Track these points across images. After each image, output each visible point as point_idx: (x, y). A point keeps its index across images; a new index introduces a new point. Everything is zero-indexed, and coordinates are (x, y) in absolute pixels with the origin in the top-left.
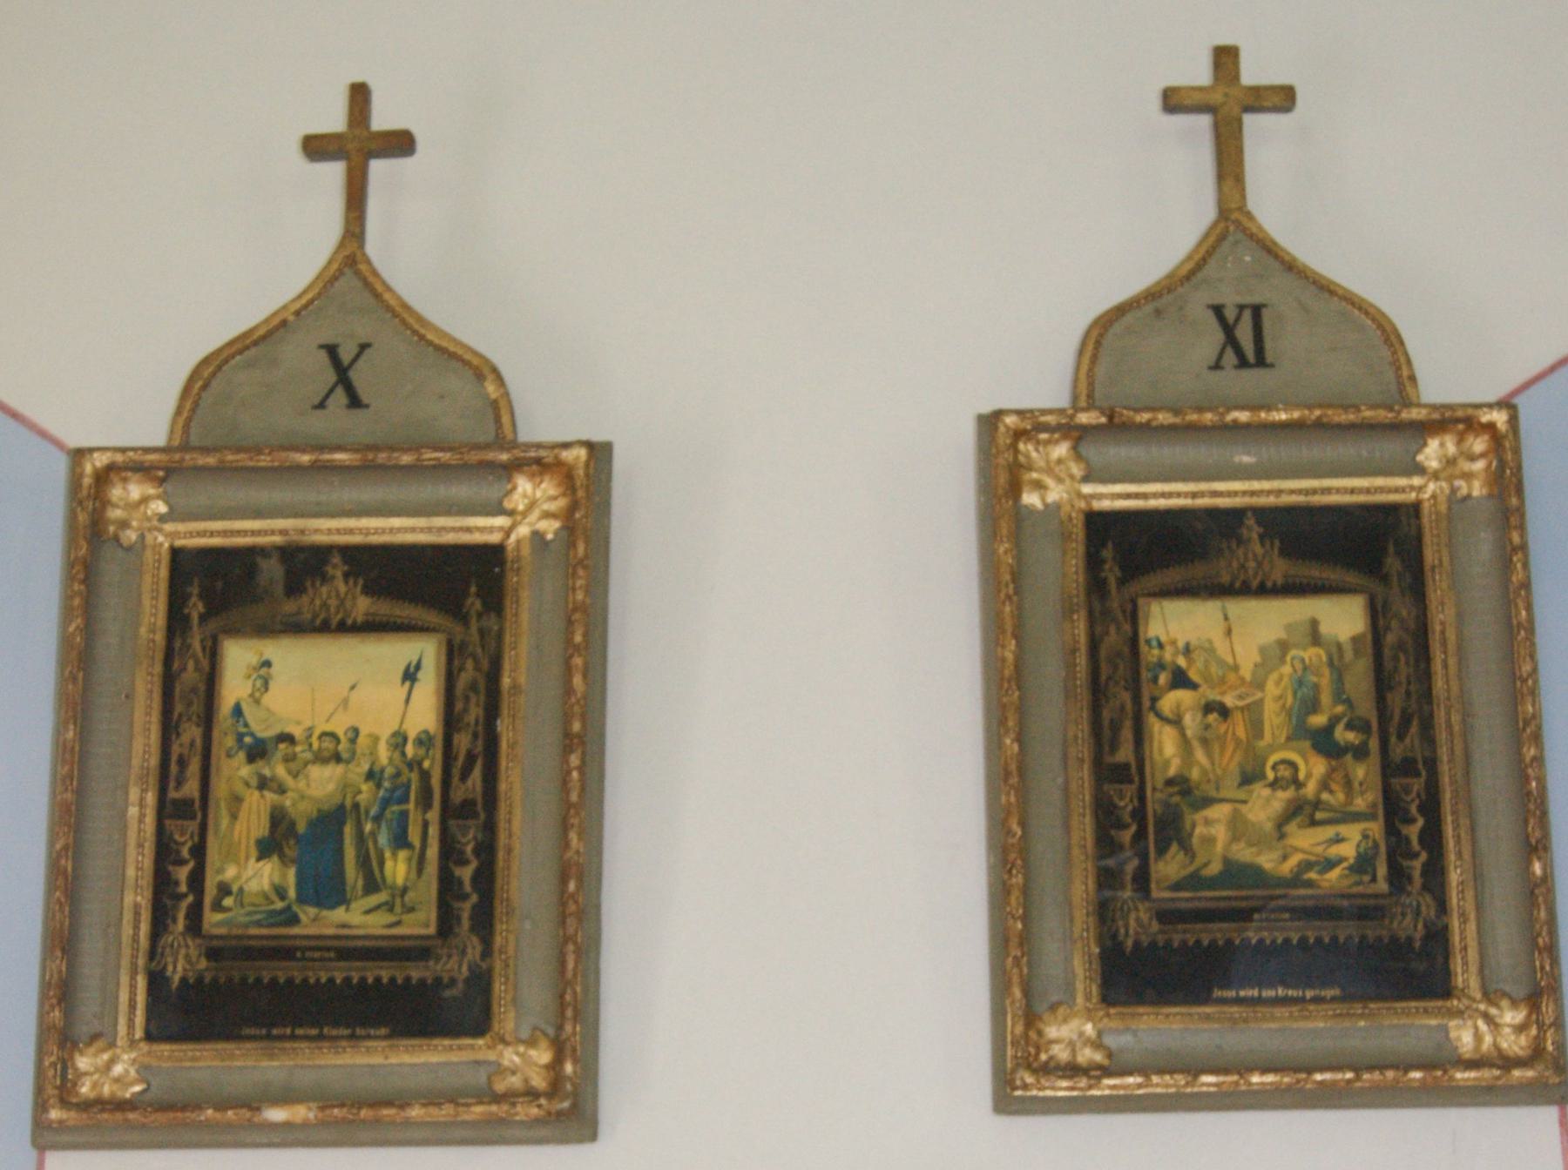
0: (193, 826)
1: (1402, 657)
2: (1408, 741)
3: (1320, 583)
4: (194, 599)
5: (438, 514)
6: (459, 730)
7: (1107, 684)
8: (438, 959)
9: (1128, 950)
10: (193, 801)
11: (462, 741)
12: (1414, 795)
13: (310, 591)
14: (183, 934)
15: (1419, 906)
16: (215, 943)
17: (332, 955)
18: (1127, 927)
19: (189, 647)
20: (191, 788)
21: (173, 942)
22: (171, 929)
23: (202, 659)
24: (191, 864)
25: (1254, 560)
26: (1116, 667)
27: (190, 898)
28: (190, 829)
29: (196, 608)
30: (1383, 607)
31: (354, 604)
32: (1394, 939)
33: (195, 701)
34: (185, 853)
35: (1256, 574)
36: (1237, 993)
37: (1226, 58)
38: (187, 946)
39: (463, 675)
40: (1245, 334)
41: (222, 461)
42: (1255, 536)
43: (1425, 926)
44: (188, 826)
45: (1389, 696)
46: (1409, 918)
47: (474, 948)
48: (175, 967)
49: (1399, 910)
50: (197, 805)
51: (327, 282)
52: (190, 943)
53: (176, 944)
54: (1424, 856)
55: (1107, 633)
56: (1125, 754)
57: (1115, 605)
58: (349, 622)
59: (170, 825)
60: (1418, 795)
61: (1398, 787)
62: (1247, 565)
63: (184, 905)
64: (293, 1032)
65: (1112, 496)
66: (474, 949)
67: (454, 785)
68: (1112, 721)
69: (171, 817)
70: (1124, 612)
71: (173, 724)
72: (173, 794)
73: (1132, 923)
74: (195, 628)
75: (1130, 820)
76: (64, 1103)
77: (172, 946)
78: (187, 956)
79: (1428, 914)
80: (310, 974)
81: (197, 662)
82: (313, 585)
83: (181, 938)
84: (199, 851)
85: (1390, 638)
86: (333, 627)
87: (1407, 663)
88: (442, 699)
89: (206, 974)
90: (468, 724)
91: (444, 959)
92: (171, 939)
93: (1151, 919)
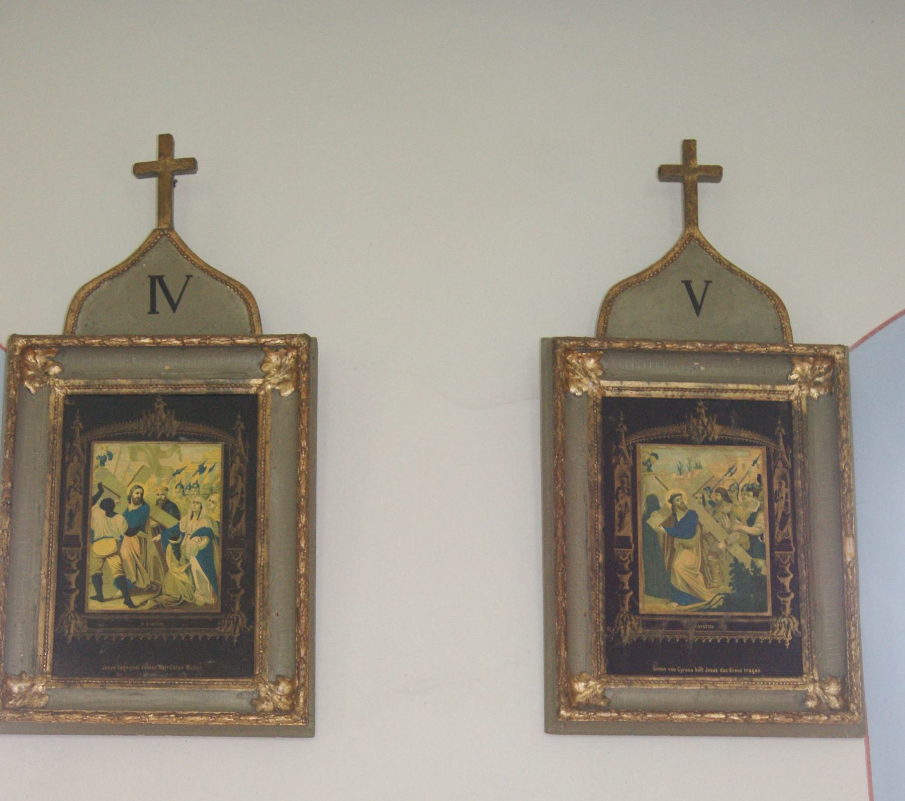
1: (240, 478)
2: (239, 526)
3: (751, 441)
4: (77, 421)
5: (671, 381)
6: (777, 501)
7: (69, 490)
8: (774, 630)
10: (78, 536)
14: (789, 616)
15: (789, 623)
16: (646, 618)
20: (77, 530)
23: (82, 454)
25: (702, 425)
28: (789, 557)
29: (78, 427)
31: (713, 429)
32: (775, 642)
34: (626, 566)
37: (689, 148)
38: (76, 620)
43: (792, 635)
44: (627, 552)
46: (783, 629)
48: (625, 631)
49: (778, 625)
50: (81, 537)
52: (78, 617)
53: (625, 619)
54: (792, 596)
56: (627, 531)
57: (623, 447)
58: (710, 439)
59: (617, 551)
60: (790, 561)
65: (631, 388)
67: (776, 532)
68: (71, 511)
69: (66, 546)
70: (629, 451)
72: (66, 533)
73: (629, 629)
74: (78, 437)
76: (570, 707)
77: (623, 619)
78: (631, 625)
81: (784, 463)
82: (146, 413)
83: (627, 615)
85: (235, 467)
87: (786, 487)
88: (90, 484)
90: (782, 497)
91: (226, 626)
92: (67, 614)
93: (638, 625)
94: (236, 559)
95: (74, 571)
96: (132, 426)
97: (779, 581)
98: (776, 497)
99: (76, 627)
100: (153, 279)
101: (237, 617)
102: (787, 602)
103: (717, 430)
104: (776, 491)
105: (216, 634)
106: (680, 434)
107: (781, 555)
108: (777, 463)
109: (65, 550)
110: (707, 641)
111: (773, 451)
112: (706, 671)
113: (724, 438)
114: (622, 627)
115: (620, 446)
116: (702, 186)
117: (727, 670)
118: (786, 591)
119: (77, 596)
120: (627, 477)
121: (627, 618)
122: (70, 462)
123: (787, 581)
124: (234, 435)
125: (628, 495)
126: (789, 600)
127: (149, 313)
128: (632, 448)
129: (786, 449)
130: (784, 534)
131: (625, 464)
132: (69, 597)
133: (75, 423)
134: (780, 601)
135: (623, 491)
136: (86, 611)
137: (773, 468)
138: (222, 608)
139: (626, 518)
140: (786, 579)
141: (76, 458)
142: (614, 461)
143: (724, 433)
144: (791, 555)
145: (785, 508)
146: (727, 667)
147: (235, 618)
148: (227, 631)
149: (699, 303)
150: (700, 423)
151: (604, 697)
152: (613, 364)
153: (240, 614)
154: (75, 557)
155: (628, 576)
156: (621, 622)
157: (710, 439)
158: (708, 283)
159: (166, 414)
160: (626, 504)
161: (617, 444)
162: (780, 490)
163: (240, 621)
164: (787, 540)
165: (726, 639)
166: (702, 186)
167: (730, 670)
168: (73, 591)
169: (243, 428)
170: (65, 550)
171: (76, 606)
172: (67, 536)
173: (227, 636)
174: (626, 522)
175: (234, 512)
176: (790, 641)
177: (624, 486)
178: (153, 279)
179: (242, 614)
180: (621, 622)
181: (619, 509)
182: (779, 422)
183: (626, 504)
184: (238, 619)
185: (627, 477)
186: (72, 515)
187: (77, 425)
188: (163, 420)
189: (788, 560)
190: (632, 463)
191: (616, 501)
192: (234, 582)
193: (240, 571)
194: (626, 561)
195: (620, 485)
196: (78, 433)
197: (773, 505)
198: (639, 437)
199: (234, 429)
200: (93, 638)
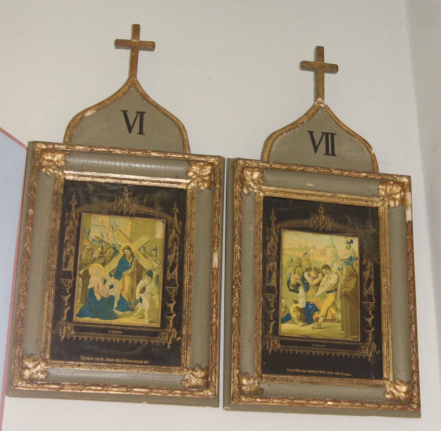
0: (70, 281)
1: (175, 244)
2: (173, 273)
3: (341, 230)
6: (365, 271)
8: (361, 349)
12: (173, 293)
13: (116, 200)
14: (371, 342)
15: (171, 332)
18: (270, 344)
20: (70, 268)
21: (62, 323)
24: (70, 295)
25: (126, 204)
27: (69, 308)
28: (174, 290)
29: (273, 219)
35: (126, 209)
36: (300, 371)
37: (320, 51)
38: (274, 339)
39: (171, 235)
42: (322, 212)
43: (372, 354)
44: (69, 281)
46: (367, 350)
47: (374, 346)
48: (62, 333)
50: (276, 288)
55: (270, 240)
56: (273, 283)
57: (274, 230)
58: (130, 213)
60: (175, 293)
61: (365, 304)
64: (94, 359)
66: (374, 347)
67: (364, 289)
68: (67, 255)
70: (276, 233)
73: (272, 344)
75: (68, 293)
77: (268, 338)
78: (67, 329)
79: (374, 349)
80: (114, 339)
81: (274, 238)
83: (65, 322)
85: (172, 236)
86: (125, 214)
89: (281, 349)
91: (163, 336)
94: (369, 309)
97: (365, 320)
98: (365, 268)
99: (67, 331)
101: (370, 345)
104: (365, 264)
105: (157, 341)
106: (307, 225)
108: (172, 230)
112: (105, 360)
114: (267, 343)
115: (271, 230)
116: (327, 75)
117: (120, 360)
118: (171, 312)
119: (68, 311)
121: (271, 337)
122: (67, 225)
124: (173, 215)
125: (73, 245)
126: (172, 317)
129: (178, 222)
130: (172, 276)
131: (274, 241)
136: (280, 334)
138: (161, 325)
140: (369, 319)
141: (71, 223)
142: (66, 223)
144: (275, 296)
145: (369, 275)
146: (340, 371)
147: (169, 332)
149: (317, 145)
150: (321, 219)
152: (269, 177)
155: (68, 297)
156: (267, 340)
157: (130, 213)
159: (325, 216)
160: (71, 251)
163: (372, 347)
165: (332, 354)
166: (327, 75)
167: (342, 373)
170: (267, 295)
172: (64, 272)
176: (170, 345)
177: (273, 255)
179: (173, 329)
180: (267, 340)
181: (269, 269)
182: (176, 205)
183: (71, 251)
184: (371, 346)
185: (74, 234)
186: (270, 273)
187: (73, 202)
188: (324, 220)
189: (371, 308)
190: (278, 241)
192: (368, 323)
195: (68, 238)
196: (273, 223)
197: (363, 274)
199: (173, 212)
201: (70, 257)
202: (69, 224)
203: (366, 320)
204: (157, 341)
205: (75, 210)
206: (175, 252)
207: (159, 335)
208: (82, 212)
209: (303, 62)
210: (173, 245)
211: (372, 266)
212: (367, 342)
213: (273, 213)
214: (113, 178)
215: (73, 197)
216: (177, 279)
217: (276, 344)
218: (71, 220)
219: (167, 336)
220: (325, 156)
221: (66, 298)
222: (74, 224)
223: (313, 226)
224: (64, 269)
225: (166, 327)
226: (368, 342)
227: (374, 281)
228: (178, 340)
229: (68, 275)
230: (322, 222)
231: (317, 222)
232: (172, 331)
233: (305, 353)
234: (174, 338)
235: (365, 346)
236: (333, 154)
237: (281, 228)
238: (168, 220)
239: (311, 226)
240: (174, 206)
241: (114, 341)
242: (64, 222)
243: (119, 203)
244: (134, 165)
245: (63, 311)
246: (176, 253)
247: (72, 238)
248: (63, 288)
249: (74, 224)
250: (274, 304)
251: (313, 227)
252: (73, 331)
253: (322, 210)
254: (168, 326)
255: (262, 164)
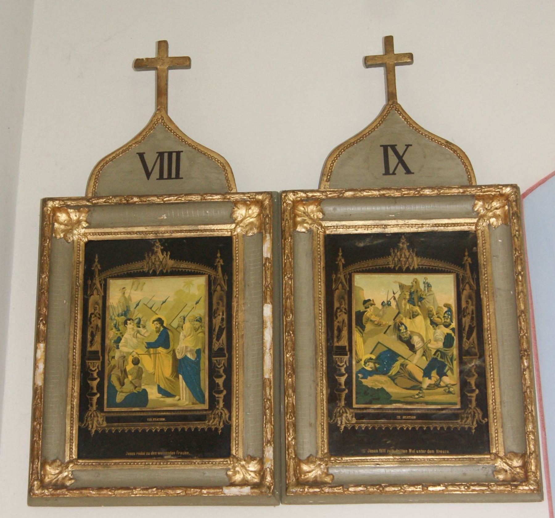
6: (465, 316)
8: (462, 419)
9: (92, 434)
10: (345, 347)
11: (466, 321)
13: (147, 259)
17: (415, 417)
19: (95, 284)
20: (96, 347)
21: (91, 415)
22: (338, 405)
24: (98, 380)
26: (341, 304)
27: (98, 395)
29: (97, 266)
30: (462, 279)
32: (210, 429)
33: (98, 308)
36: (146, 454)
38: (98, 417)
39: (465, 292)
40: (393, 160)
41: (307, 196)
43: (224, 423)
45: (464, 319)
47: (479, 414)
49: (213, 416)
50: (347, 348)
51: (152, 126)
54: (225, 392)
57: (342, 276)
58: (411, 268)
60: (224, 365)
61: (337, 359)
62: (401, 259)
63: (95, 399)
66: (479, 414)
68: (338, 326)
69: (89, 359)
71: (89, 319)
72: (89, 349)
73: (95, 423)
75: (96, 377)
77: (340, 413)
79: (479, 417)
83: (95, 413)
84: (101, 374)
85: (465, 294)
86: (404, 270)
90: (469, 314)
91: (465, 419)
93: (103, 421)
95: (95, 379)
96: (135, 266)
97: (215, 381)
100: (385, 148)
102: (220, 397)
103: (416, 262)
107: (217, 360)
109: (89, 363)
110: (408, 428)
111: (462, 277)
112: (368, 452)
113: (422, 267)
117: (377, 450)
118: (472, 387)
119: (98, 399)
120: (98, 305)
121: (343, 411)
123: (220, 381)
125: (345, 313)
126: (474, 395)
127: (384, 174)
128: (348, 277)
132: (91, 399)
133: (95, 265)
134: (215, 396)
135: (341, 311)
137: (461, 290)
139: (343, 332)
142: (334, 287)
143: (175, 266)
145: (221, 323)
147: (220, 414)
148: (213, 424)
150: (403, 255)
151: (327, 474)
152: (98, 216)
153: (223, 410)
154: (344, 363)
156: (338, 414)
157: (411, 268)
158: (408, 146)
159: (163, 255)
160: (344, 321)
161: (336, 274)
162: (467, 307)
163: (476, 415)
164: (222, 348)
168: (95, 394)
169: (470, 262)
170: (89, 363)
171: (97, 406)
173: (213, 427)
174: (343, 335)
175: (467, 328)
176: (475, 428)
177: (342, 306)
178: (385, 148)
179: (477, 409)
184: (474, 413)
185: (98, 305)
189: (222, 365)
191: (89, 323)
192: (218, 384)
193: (474, 375)
194: (343, 365)
195: (93, 311)
196: (97, 273)
198: (110, 273)
199: (464, 263)
200: (110, 431)
201: (96, 333)
202: (338, 289)
203: (217, 382)
204: (205, 427)
205: (343, 271)
206: (221, 314)
207: (207, 419)
208: (352, 272)
209: (411, 63)
210: (468, 304)
211: (474, 310)
212: (469, 409)
213: (340, 254)
214: (137, 233)
215: (339, 255)
216: (225, 347)
217: (350, 419)
218: (218, 285)
219: (470, 419)
220: (385, 176)
221: (94, 384)
222: (223, 289)
223: (393, 266)
224: (336, 344)
225: (468, 407)
226: (218, 409)
227: (227, 330)
228: (484, 422)
229: (94, 355)
230: (405, 259)
231: (399, 260)
232: (476, 412)
233: (442, 428)
234: (225, 421)
235: (214, 415)
236: (178, 176)
237: (352, 272)
238: (459, 273)
239: (390, 266)
240: (465, 256)
241: (405, 429)
242: (332, 286)
243: (150, 261)
244: (355, 209)
245: (340, 395)
246: (223, 315)
247: (98, 310)
248: (89, 371)
249: (223, 289)
250: (346, 369)
251: (394, 267)
252: (105, 422)
253: (158, 248)
254: (217, 407)
255: (406, 192)
